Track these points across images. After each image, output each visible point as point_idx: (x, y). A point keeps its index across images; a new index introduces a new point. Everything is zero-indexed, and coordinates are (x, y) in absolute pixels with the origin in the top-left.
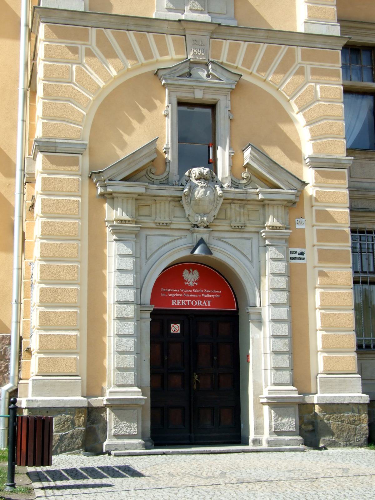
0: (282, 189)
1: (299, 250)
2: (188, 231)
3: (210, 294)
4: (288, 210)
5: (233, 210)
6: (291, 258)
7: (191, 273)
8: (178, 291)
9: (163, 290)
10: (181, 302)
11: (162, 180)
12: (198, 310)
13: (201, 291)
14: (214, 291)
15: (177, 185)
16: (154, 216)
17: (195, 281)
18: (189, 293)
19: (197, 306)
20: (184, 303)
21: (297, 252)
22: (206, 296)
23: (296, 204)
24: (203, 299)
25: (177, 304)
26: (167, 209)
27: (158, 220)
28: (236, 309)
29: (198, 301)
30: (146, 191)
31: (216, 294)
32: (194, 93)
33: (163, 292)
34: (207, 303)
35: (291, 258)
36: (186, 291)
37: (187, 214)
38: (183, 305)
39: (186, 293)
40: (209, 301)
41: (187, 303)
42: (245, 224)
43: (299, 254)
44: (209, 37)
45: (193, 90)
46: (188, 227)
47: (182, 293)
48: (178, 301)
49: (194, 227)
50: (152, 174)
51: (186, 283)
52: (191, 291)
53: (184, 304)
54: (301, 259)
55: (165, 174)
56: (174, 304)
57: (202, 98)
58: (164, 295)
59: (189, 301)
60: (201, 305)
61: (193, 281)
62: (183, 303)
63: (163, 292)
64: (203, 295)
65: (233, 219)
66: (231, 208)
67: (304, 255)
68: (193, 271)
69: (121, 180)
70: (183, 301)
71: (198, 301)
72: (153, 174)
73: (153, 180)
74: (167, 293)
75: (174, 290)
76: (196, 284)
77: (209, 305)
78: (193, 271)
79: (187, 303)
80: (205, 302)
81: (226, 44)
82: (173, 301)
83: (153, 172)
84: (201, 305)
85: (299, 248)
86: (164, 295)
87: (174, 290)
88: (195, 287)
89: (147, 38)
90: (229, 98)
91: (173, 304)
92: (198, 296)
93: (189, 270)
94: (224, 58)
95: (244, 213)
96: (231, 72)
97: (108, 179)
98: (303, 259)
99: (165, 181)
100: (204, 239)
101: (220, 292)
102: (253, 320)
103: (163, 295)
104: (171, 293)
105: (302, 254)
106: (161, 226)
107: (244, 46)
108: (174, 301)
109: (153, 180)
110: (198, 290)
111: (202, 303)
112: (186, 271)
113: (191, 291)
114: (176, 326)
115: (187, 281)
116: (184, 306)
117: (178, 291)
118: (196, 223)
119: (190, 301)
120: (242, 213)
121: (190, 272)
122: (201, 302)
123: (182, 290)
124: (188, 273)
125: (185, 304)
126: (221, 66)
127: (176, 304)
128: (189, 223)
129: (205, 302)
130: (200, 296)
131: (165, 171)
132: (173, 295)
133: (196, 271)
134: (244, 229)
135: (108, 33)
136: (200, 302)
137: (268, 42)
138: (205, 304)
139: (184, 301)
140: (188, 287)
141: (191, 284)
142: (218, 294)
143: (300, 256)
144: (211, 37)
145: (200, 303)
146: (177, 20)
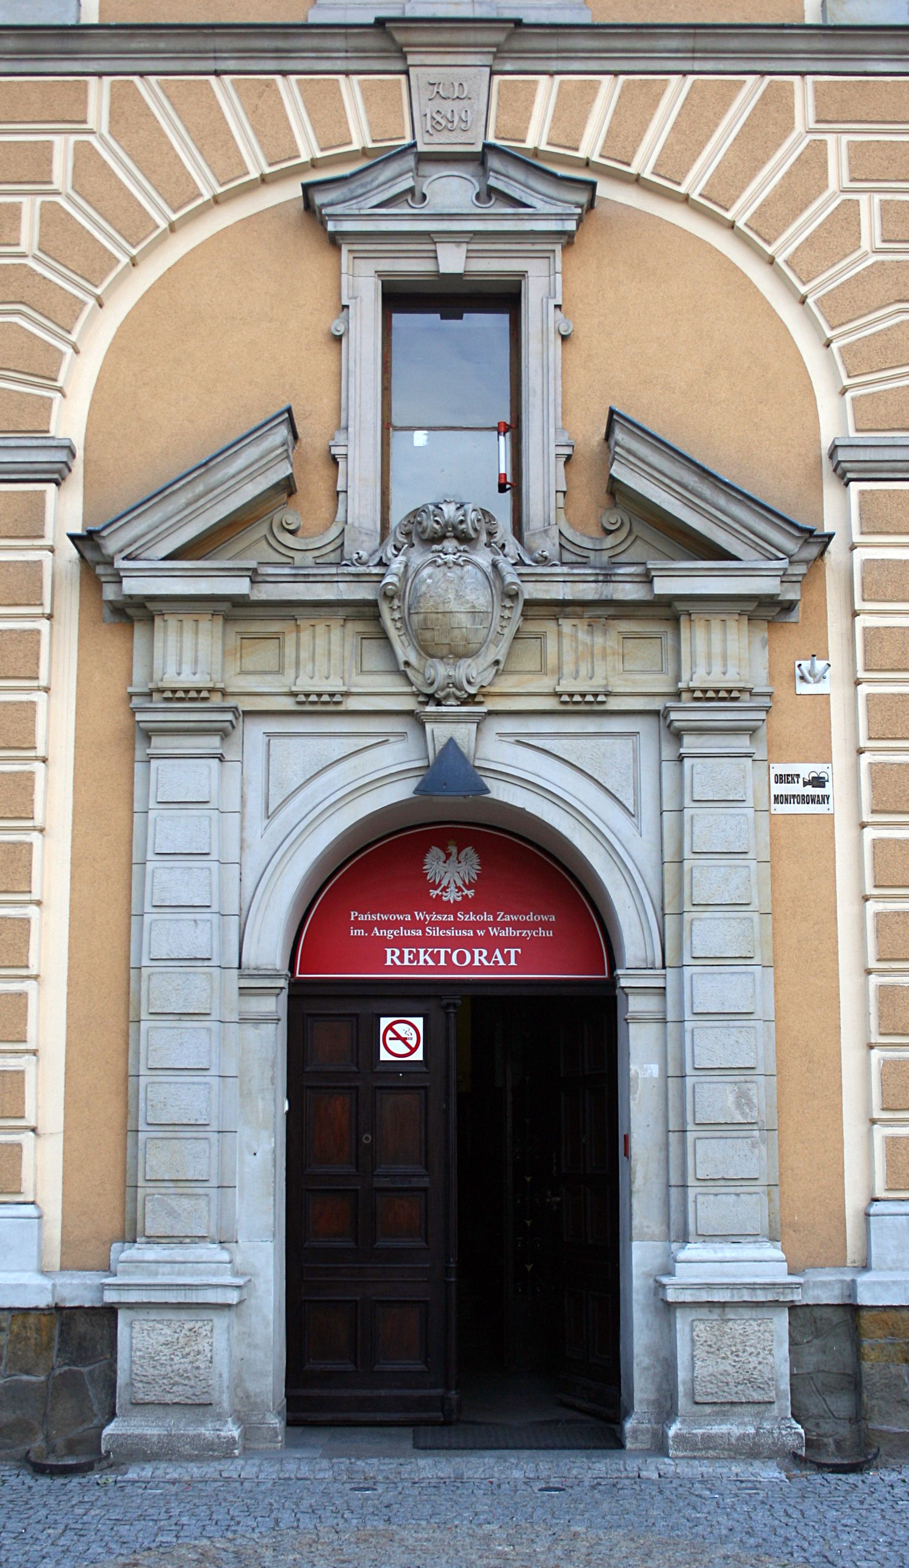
0: (735, 558)
1: (806, 770)
2: (408, 719)
3: (516, 925)
4: (766, 635)
5: (566, 642)
6: (776, 798)
7: (453, 858)
8: (451, 918)
9: (356, 918)
10: (417, 956)
11: (324, 551)
12: (474, 979)
13: (486, 917)
14: (531, 917)
15: (362, 564)
16: (290, 672)
17: (465, 884)
18: (444, 925)
19: (470, 968)
20: (427, 957)
21: (798, 776)
22: (502, 934)
23: (795, 616)
24: (491, 944)
25: (402, 961)
26: (336, 648)
27: (304, 684)
28: (606, 976)
29: (476, 951)
30: (252, 588)
31: (540, 924)
32: (436, 258)
33: (358, 924)
34: (506, 958)
35: (776, 798)
36: (435, 917)
37: (402, 658)
38: (422, 963)
39: (433, 924)
40: (513, 951)
41: (435, 957)
42: (607, 685)
43: (805, 784)
44: (487, 70)
45: (432, 247)
46: (408, 704)
47: (421, 925)
48: (406, 951)
49: (426, 703)
50: (288, 535)
51: (434, 893)
52: (409, 918)
53: (425, 961)
54: (812, 799)
55: (334, 532)
56: (392, 961)
57: (462, 271)
58: (361, 932)
59: (442, 951)
60: (486, 963)
61: (460, 883)
62: (424, 958)
63: (358, 924)
64: (493, 931)
65: (568, 668)
66: (560, 634)
67: (824, 786)
68: (459, 852)
69: (164, 559)
70: (422, 951)
71: (476, 951)
72: (292, 532)
73: (291, 553)
74: (368, 926)
75: (393, 917)
76: (471, 893)
77: (513, 963)
78: (459, 852)
79: (435, 957)
80: (497, 952)
81: (546, 91)
82: (389, 951)
83: (291, 527)
84: (486, 963)
85: (807, 760)
86: (361, 932)
87: (393, 917)
88: (465, 905)
89: (277, 91)
90: (559, 267)
91: (389, 963)
92: (475, 933)
93: (443, 848)
94: (536, 137)
95: (604, 649)
96: (553, 175)
97: (124, 554)
98: (824, 799)
99: (332, 555)
100: (458, 741)
101: (553, 919)
102: (638, 1020)
103: (354, 932)
104: (382, 925)
105: (818, 782)
106: (313, 703)
107: (609, 90)
108: (393, 953)
109: (291, 553)
110: (475, 913)
111: (488, 958)
112: (435, 851)
113: (451, 918)
114: (401, 1029)
115: (440, 884)
116: (426, 969)
117: (409, 918)
118: (430, 691)
119: (446, 952)
120: (597, 650)
121: (448, 856)
122: (485, 953)
123: (419, 916)
124: (443, 857)
125: (431, 963)
126: (529, 163)
127: (398, 963)
128: (408, 689)
129: (497, 952)
130: (481, 933)
131: (334, 520)
132: (390, 934)
133: (469, 850)
134: (603, 703)
135: (149, 90)
136: (481, 954)
137: (697, 68)
138: (500, 959)
139: (425, 953)
140: (440, 906)
141: (452, 896)
142: (546, 926)
143: (810, 790)
144: (496, 68)
145: (482, 958)
146: (371, 21)
